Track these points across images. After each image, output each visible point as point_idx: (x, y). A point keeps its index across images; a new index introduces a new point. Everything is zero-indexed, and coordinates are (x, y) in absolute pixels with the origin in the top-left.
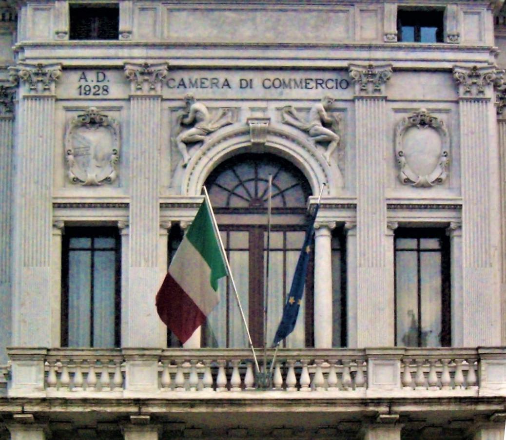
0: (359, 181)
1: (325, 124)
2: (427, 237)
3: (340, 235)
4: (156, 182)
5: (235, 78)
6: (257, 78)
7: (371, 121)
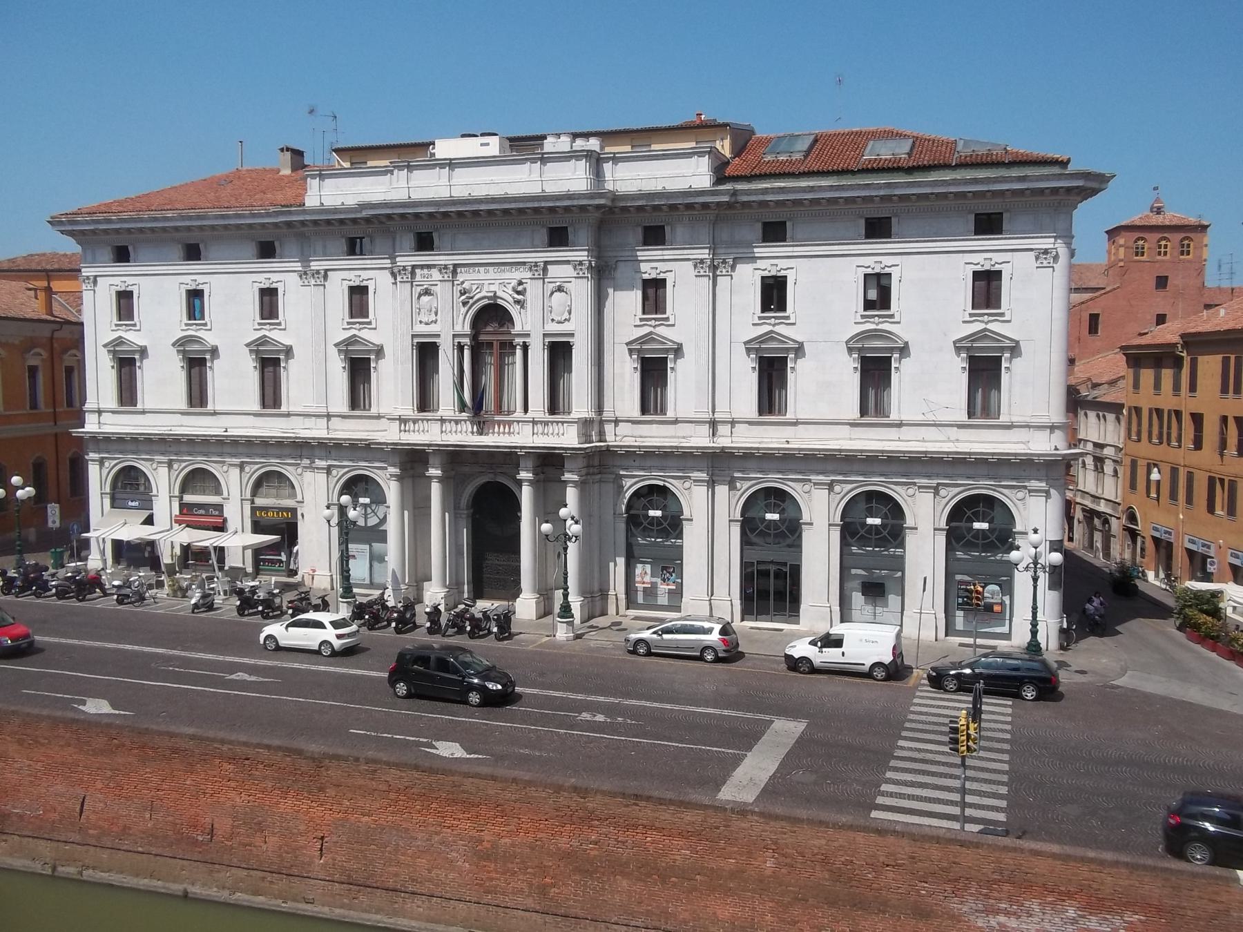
0: (530, 323)
1: (518, 293)
2: (559, 352)
3: (525, 348)
4: (450, 325)
5: (482, 269)
6: (491, 269)
7: (534, 290)
